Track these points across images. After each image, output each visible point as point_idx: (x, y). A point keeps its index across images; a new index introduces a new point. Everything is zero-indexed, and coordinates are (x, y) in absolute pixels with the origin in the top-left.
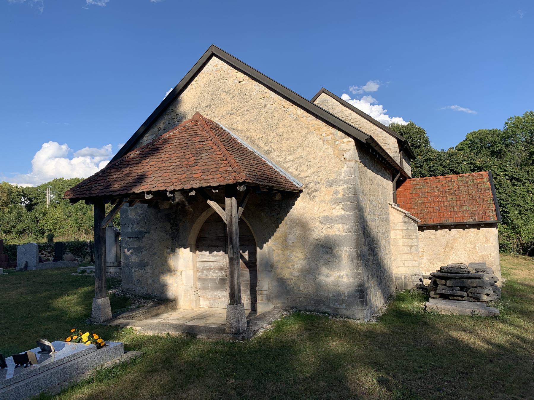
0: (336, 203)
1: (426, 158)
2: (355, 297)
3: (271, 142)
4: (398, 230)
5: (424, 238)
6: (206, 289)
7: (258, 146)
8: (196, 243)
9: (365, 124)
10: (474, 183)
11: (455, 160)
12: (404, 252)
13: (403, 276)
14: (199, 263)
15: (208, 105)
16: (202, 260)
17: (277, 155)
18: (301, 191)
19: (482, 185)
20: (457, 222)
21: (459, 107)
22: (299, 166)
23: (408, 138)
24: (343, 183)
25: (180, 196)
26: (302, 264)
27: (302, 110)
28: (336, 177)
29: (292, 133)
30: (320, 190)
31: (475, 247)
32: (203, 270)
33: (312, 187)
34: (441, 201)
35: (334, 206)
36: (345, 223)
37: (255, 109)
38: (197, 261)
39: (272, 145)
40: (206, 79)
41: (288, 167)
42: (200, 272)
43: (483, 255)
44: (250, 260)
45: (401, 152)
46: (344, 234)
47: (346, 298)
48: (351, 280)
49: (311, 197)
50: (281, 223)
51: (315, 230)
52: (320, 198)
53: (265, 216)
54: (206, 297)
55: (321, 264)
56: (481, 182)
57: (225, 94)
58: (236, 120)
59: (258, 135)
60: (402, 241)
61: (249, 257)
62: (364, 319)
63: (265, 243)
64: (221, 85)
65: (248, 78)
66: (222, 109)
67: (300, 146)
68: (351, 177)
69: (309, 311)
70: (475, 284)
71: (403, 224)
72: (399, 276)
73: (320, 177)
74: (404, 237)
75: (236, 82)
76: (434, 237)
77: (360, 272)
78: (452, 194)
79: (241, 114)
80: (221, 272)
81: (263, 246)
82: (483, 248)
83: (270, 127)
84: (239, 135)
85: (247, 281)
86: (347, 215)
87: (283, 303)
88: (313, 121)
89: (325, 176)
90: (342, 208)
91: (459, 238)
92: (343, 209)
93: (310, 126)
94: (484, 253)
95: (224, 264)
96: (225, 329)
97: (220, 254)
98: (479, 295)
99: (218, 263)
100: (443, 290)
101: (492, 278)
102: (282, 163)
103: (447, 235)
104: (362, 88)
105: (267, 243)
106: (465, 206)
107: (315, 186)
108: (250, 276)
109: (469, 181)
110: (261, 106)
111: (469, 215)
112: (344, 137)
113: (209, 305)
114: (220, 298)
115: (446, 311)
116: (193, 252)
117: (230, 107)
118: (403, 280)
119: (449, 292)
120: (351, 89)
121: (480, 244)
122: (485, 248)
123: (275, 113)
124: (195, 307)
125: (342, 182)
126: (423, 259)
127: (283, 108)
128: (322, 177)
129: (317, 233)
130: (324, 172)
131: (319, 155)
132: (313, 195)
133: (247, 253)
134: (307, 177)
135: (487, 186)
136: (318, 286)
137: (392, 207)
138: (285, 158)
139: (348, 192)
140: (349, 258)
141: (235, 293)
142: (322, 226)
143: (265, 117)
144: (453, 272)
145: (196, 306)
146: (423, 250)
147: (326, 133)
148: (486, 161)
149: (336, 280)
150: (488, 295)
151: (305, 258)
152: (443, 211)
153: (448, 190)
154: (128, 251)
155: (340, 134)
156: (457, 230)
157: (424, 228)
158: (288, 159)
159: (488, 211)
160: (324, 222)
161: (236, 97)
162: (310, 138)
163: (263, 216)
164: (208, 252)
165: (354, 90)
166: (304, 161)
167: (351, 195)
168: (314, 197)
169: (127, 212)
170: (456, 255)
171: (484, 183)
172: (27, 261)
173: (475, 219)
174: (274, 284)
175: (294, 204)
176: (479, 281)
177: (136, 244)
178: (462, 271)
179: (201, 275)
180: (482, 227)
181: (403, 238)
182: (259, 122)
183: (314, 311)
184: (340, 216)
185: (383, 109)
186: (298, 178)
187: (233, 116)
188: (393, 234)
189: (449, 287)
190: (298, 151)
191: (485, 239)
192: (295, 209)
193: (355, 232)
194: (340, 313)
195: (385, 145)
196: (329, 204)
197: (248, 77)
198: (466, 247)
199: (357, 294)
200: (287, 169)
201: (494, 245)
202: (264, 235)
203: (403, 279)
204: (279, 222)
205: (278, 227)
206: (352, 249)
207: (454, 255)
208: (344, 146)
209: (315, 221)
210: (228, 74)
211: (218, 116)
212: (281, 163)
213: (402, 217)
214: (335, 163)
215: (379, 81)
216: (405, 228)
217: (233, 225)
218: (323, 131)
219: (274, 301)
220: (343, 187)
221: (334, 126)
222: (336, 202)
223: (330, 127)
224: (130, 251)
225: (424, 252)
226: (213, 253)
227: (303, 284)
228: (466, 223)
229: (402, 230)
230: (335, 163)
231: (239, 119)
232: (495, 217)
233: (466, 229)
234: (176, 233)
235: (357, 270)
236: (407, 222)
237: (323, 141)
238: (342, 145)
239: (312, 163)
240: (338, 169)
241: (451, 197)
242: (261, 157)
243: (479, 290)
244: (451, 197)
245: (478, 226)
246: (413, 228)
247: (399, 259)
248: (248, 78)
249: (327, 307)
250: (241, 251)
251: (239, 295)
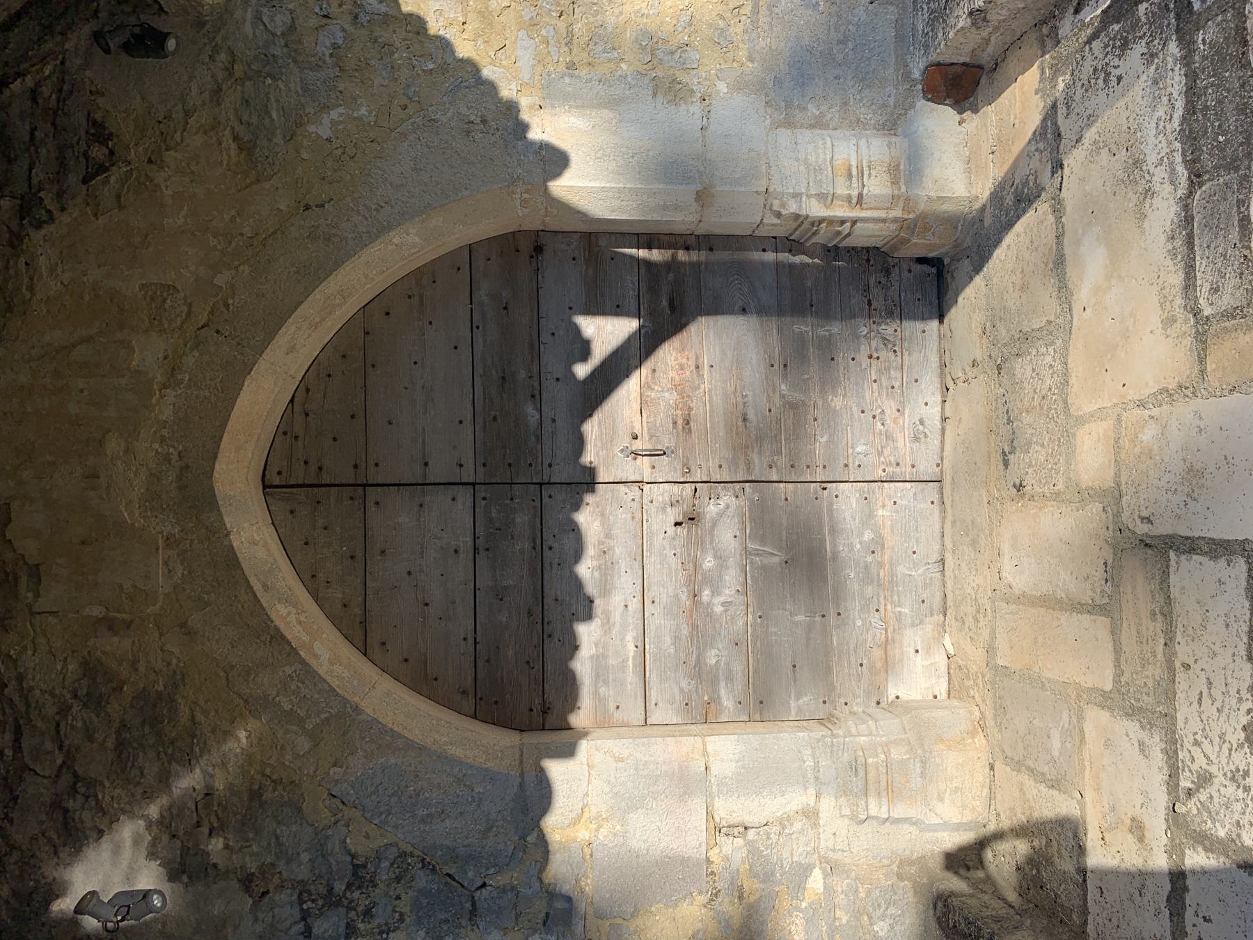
14: (651, 706)
16: (631, 678)
25: (116, 851)
32: (699, 672)
42: (715, 699)
44: (633, 304)
53: (334, 114)
54: (877, 653)
61: (617, 310)
63: (525, 127)
80: (714, 524)
105: (525, 116)
113: (929, 628)
133: (589, 326)
163: (333, 122)
179: (739, 687)
202: (468, 127)
205: (416, 25)
226: (591, 589)
234: (422, 879)
250: (582, 370)
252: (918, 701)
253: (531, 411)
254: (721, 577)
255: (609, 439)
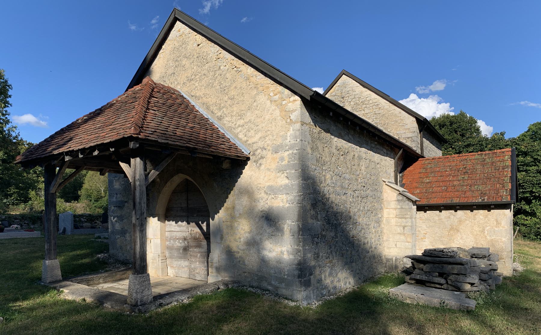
0: (281, 171)
1: (466, 144)
2: (294, 276)
3: (223, 107)
4: (392, 208)
5: (426, 219)
6: (172, 258)
7: (212, 112)
8: (166, 213)
9: (384, 104)
10: (493, 161)
11: (497, 145)
12: (397, 233)
13: (394, 258)
15: (172, 73)
16: (170, 229)
17: (228, 120)
18: (248, 159)
19: (502, 163)
20: (462, 202)
21: (530, 102)
22: (247, 132)
23: (458, 128)
24: (289, 148)
26: (247, 237)
27: (252, 69)
28: (282, 142)
29: (242, 95)
30: (266, 157)
31: (483, 231)
33: (259, 154)
34: (450, 181)
35: (279, 174)
36: (288, 194)
37: (210, 72)
38: (167, 230)
39: (224, 109)
40: (171, 46)
41: (238, 133)
43: (492, 239)
45: (422, 133)
46: (288, 205)
47: (286, 277)
48: (292, 257)
49: (258, 164)
50: (230, 193)
51: (260, 201)
52: (265, 166)
53: (216, 186)
55: (265, 238)
56: (501, 160)
57: (186, 59)
58: (195, 86)
59: (213, 100)
60: (395, 220)
62: (302, 301)
64: (183, 50)
65: (205, 39)
66: (183, 76)
67: (249, 109)
68: (297, 141)
69: (253, 287)
70: (455, 270)
71: (397, 202)
72: (390, 257)
73: (267, 143)
74: (397, 216)
75: (195, 45)
76: (437, 219)
77: (300, 248)
78: (464, 173)
79: (198, 80)
80: (184, 243)
81: (215, 217)
82: (493, 232)
83: (224, 90)
84: (197, 102)
85: (205, 252)
86: (291, 185)
87: (230, 277)
88: (262, 80)
89: (271, 141)
90: (286, 177)
91: (466, 220)
92: (288, 178)
93: (259, 86)
94: (493, 238)
95: (186, 234)
96: (126, 300)
97: (184, 225)
98: (459, 284)
99: (182, 234)
100: (418, 276)
101: (490, 265)
102: (233, 129)
103: (452, 217)
104: (428, 88)
105: (218, 214)
106: (477, 185)
107: (261, 153)
108: (207, 247)
109: (488, 159)
110: (216, 69)
111: (479, 195)
112: (290, 95)
113: (175, 274)
114: (183, 268)
115: (411, 299)
116: (160, 221)
117: (190, 72)
118: (394, 262)
119: (424, 278)
120: (418, 89)
121: (489, 227)
122: (494, 232)
123: (228, 75)
124: (161, 275)
125: (287, 147)
126: (425, 241)
127: (235, 69)
128: (268, 143)
129: (262, 204)
130: (271, 137)
131: (267, 117)
132: (259, 162)
134: (254, 143)
135: (507, 164)
136: (263, 261)
137: (386, 184)
138: (235, 123)
139: (293, 158)
140: (290, 232)
141: (137, 263)
142: (267, 197)
143: (219, 80)
144: (433, 255)
145: (162, 274)
146: (425, 232)
147: (274, 92)
148: (532, 146)
149: (278, 255)
150: (472, 284)
151: (251, 231)
152: (449, 191)
153: (461, 169)
154: (114, 219)
155: (287, 92)
156: (464, 212)
157: (426, 208)
158: (238, 124)
159: (501, 191)
160: (269, 193)
161: (195, 62)
162: (258, 99)
164: (174, 222)
165: (421, 89)
166: (252, 126)
167: (296, 162)
168: (260, 164)
169: (113, 183)
170: (461, 238)
171: (504, 161)
172: (65, 227)
173: (484, 200)
174: (223, 257)
175: (241, 173)
176: (461, 268)
177: (119, 213)
178: (443, 255)
179: (169, 245)
180: (493, 209)
181: (396, 217)
182: (214, 86)
183: (257, 287)
184: (285, 185)
185: (450, 107)
186: (246, 145)
187: (193, 82)
188: (386, 213)
189: (426, 272)
190: (247, 115)
191: (495, 222)
192: (243, 178)
193: (298, 203)
194: (279, 293)
195: (404, 125)
196: (273, 174)
197: (205, 38)
198: (473, 231)
199: (296, 273)
200: (236, 136)
201: (506, 229)
202: (216, 206)
203: (394, 260)
204: (229, 192)
205: (227, 197)
206: (294, 222)
207: (459, 238)
208: (291, 106)
209: (261, 191)
210: (189, 37)
211: (180, 84)
212: (231, 129)
213: (396, 195)
214: (281, 127)
215: (446, 80)
216: (399, 207)
217: (137, 189)
218: (271, 90)
219: (223, 274)
220: (288, 153)
221: (281, 84)
222: (281, 170)
223: (278, 85)
224: (115, 219)
225: (426, 234)
226: (178, 223)
227: (248, 258)
228: (473, 204)
229: (395, 209)
230: (281, 127)
231: (197, 85)
232: (509, 197)
233: (474, 211)
235: (297, 246)
236: (402, 200)
237: (271, 101)
238: (289, 104)
239: (260, 127)
240: (284, 133)
241: (463, 176)
242: (214, 124)
243: (461, 278)
244: (463, 176)
245: (488, 207)
246: (407, 207)
247: (391, 239)
248: (205, 40)
249: (269, 284)
250: (200, 222)
251: (143, 264)
252: (440, 134)
253: (195, 215)
254: (231, 227)
255: (193, 227)
